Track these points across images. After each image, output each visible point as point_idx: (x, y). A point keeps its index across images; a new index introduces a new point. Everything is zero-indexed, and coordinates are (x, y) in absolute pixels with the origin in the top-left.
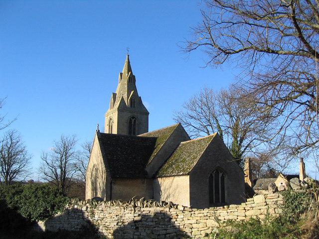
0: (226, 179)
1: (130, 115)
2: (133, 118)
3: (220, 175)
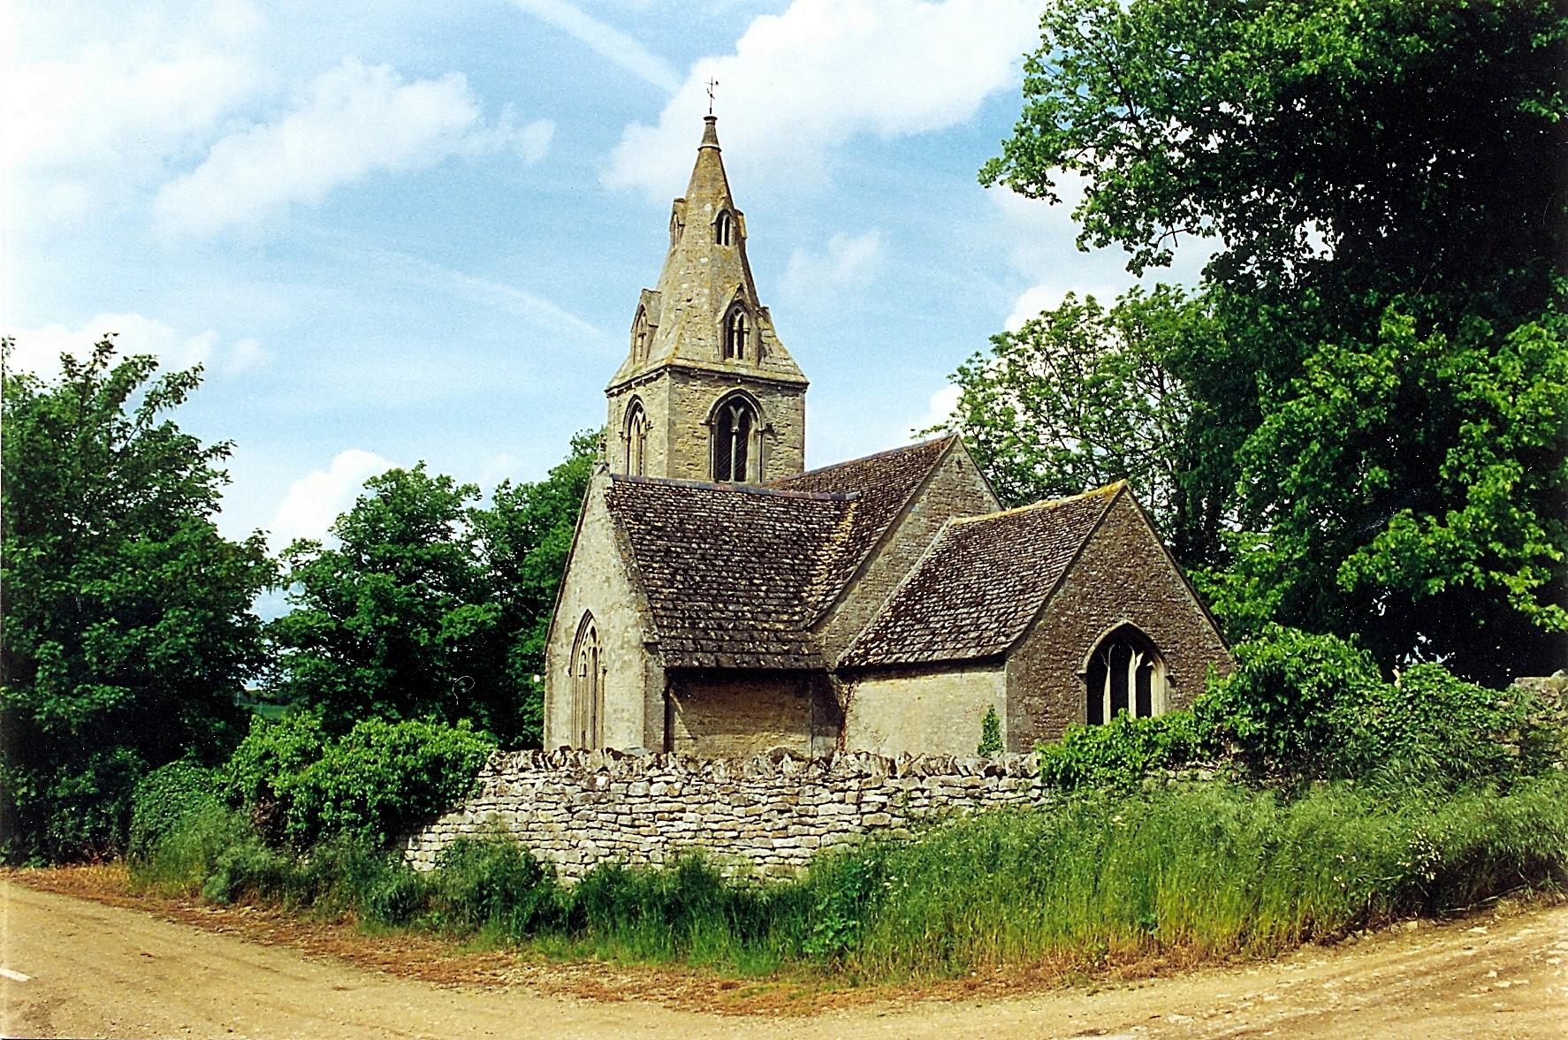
0: (1158, 681)
1: (724, 391)
2: (738, 403)
3: (1135, 662)
